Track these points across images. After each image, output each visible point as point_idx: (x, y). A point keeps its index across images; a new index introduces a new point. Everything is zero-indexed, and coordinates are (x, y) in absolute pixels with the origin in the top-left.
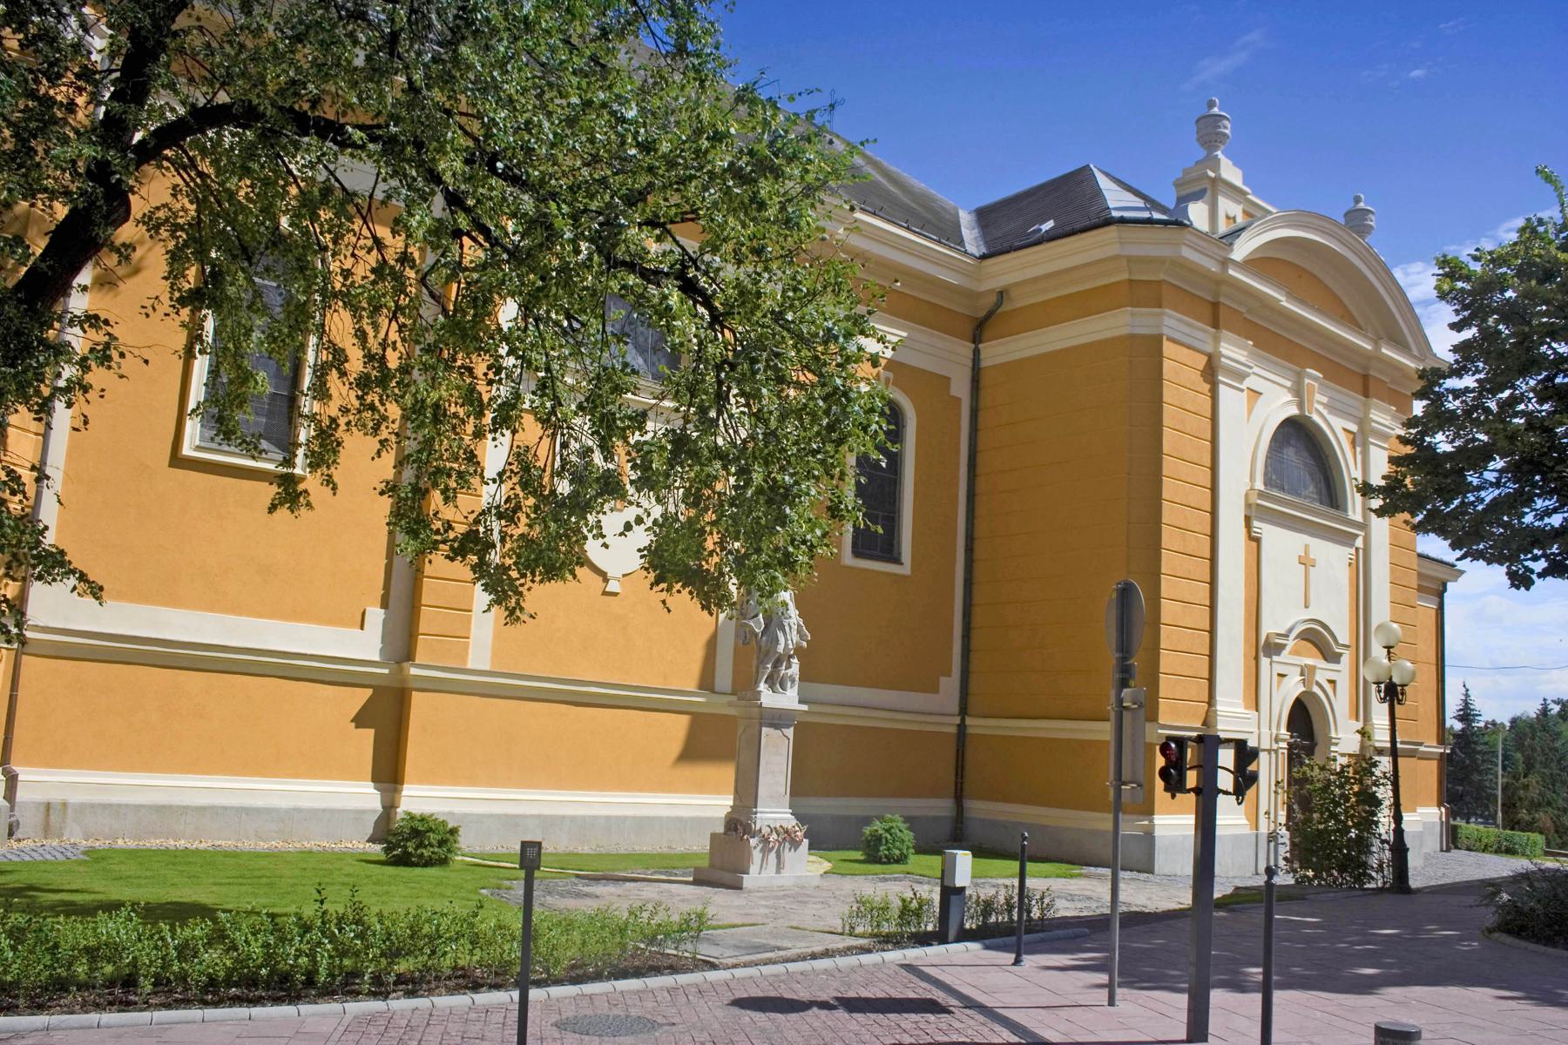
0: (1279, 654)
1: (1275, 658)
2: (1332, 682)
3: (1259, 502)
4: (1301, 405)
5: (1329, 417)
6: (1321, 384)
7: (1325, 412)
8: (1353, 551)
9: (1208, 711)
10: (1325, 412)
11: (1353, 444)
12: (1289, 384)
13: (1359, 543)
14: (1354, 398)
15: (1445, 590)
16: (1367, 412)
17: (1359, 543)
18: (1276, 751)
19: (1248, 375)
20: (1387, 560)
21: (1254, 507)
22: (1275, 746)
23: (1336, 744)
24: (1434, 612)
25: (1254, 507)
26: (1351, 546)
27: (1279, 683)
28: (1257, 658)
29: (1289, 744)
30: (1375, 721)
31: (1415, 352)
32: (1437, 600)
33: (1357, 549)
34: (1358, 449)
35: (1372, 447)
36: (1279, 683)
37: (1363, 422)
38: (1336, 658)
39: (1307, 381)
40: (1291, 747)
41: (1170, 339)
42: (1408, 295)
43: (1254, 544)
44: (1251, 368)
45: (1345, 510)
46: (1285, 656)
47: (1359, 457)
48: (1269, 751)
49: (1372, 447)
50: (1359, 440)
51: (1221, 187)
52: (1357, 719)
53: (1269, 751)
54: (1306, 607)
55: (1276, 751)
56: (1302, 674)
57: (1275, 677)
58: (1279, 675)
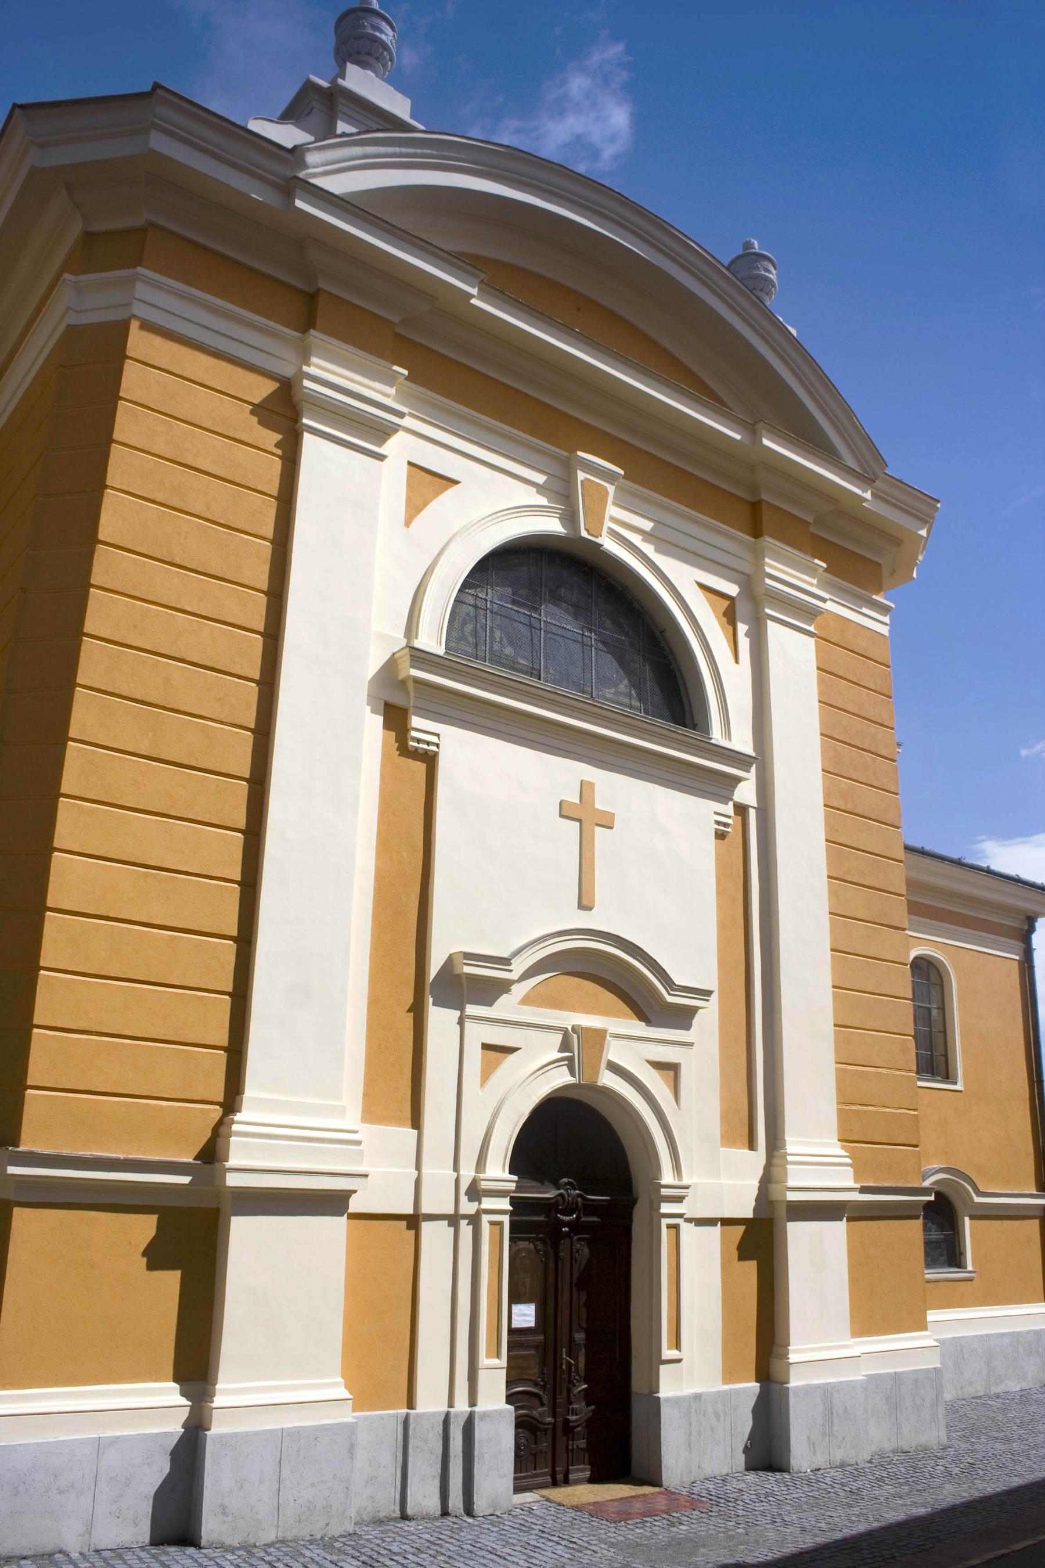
0: (489, 1003)
1: (471, 1009)
2: (670, 1069)
3: (415, 673)
4: (570, 518)
5: (660, 560)
6: (619, 489)
7: (648, 549)
8: (729, 809)
9: (220, 1123)
10: (648, 549)
11: (730, 617)
12: (540, 479)
13: (746, 792)
14: (732, 538)
15: (1032, 929)
16: (759, 566)
17: (746, 792)
18: (474, 1220)
19: (394, 429)
20: (822, 836)
21: (411, 685)
22: (468, 1207)
23: (679, 1199)
24: (1015, 966)
25: (411, 685)
26: (725, 799)
27: (486, 1074)
28: (418, 1011)
29: (514, 1201)
30: (790, 1149)
31: (851, 462)
32: (1020, 945)
33: (741, 810)
34: (742, 628)
35: (770, 624)
36: (486, 1074)
37: (750, 583)
38: (683, 1017)
39: (581, 475)
40: (519, 1205)
41: (147, 326)
42: (543, 154)
43: (420, 767)
44: (401, 415)
45: (706, 730)
46: (505, 1006)
47: (744, 643)
48: (453, 1220)
49: (770, 624)
50: (741, 609)
51: (342, 106)
52: (752, 1145)
53: (453, 1220)
54: (581, 906)
55: (474, 1220)
56: (565, 1046)
57: (474, 1056)
58: (486, 1047)
